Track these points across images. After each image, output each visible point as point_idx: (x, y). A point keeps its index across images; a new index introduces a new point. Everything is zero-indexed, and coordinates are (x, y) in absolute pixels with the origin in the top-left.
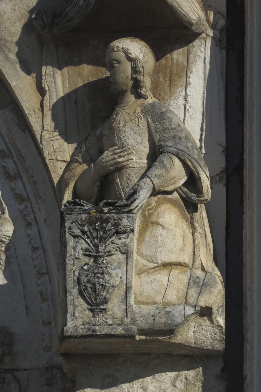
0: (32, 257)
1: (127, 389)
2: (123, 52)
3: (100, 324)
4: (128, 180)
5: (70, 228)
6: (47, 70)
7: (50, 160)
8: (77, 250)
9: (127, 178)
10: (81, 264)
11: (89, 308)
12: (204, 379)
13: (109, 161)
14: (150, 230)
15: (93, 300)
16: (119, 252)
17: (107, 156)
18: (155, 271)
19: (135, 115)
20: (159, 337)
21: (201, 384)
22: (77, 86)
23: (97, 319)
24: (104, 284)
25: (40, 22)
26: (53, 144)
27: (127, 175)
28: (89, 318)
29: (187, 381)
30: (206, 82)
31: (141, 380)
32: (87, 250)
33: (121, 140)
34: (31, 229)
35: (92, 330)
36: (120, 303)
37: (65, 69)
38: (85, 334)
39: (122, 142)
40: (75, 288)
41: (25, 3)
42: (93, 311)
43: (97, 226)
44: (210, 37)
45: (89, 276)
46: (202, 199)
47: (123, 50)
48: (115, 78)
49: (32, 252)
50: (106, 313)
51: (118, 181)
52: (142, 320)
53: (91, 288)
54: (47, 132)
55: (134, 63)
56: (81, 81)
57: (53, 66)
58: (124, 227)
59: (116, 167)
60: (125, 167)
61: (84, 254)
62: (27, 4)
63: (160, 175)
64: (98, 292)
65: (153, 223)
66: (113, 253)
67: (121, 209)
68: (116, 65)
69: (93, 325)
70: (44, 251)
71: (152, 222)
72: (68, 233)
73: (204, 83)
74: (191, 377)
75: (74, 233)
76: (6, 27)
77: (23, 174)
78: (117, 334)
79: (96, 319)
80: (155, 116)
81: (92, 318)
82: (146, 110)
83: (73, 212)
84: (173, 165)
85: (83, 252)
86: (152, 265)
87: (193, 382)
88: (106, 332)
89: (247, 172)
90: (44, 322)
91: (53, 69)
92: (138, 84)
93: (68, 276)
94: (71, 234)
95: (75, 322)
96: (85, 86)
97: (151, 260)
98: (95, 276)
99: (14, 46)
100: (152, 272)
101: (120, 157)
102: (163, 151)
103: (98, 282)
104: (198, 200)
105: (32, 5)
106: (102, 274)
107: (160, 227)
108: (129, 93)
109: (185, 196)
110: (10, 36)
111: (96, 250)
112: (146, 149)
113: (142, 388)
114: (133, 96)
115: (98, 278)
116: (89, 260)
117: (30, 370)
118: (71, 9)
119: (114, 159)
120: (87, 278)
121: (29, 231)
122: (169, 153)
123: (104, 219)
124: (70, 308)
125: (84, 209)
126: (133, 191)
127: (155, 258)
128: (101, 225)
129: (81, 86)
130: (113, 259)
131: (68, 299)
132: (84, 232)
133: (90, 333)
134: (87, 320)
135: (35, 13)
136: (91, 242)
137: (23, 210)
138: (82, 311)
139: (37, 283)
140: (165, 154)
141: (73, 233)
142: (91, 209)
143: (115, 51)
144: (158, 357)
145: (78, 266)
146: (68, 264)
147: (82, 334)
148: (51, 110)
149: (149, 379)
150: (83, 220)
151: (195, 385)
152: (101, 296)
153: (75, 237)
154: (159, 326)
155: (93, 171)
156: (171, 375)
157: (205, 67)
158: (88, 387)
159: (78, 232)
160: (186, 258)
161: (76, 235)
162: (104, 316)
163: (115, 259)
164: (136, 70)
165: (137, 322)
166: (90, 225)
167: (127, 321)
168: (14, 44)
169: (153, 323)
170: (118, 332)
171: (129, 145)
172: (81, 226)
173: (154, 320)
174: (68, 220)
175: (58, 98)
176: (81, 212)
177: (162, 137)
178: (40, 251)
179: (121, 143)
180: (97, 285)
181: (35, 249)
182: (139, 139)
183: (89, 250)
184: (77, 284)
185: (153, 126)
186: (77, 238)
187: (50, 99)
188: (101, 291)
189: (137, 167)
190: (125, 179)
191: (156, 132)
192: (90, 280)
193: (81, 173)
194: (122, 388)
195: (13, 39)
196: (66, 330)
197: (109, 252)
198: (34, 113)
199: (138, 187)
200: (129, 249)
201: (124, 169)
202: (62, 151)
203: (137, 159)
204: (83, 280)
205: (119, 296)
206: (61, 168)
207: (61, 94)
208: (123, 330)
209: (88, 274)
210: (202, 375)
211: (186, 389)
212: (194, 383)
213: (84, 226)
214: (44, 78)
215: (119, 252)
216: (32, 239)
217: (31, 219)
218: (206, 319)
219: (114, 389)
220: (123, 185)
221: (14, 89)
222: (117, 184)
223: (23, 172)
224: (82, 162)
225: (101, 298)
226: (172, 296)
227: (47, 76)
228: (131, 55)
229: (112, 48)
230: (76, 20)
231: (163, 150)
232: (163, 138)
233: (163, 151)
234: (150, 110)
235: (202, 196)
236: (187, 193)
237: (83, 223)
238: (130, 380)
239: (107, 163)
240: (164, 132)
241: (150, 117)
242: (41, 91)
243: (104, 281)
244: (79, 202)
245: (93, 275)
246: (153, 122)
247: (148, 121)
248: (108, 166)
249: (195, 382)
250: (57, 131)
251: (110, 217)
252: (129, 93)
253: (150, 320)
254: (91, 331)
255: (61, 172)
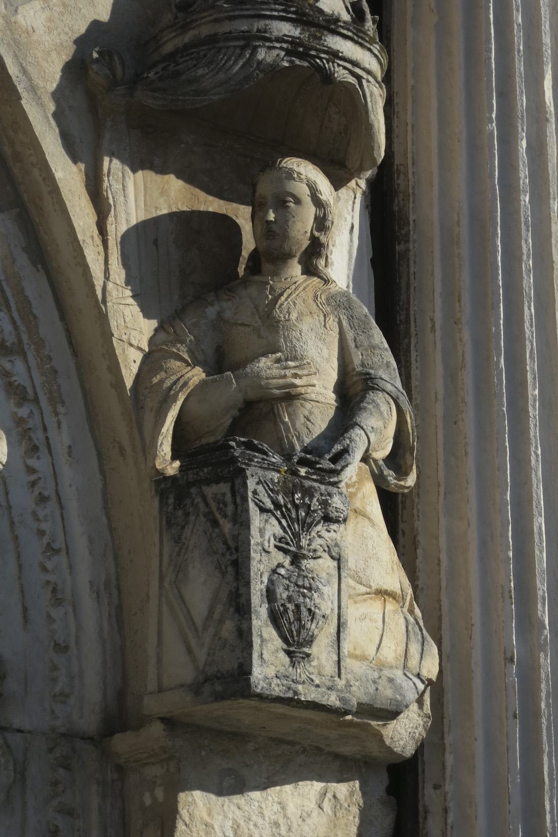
0: (34, 514)
1: (258, 802)
2: (308, 185)
3: (304, 681)
4: (308, 423)
5: (255, 492)
6: (112, 167)
7: (119, 342)
8: (266, 535)
9: (305, 417)
10: (272, 563)
11: (284, 648)
12: (365, 803)
13: (275, 378)
14: (353, 523)
15: (295, 635)
16: (326, 555)
18: (365, 600)
19: (318, 306)
20: (372, 721)
21: (358, 811)
22: (160, 213)
23: (298, 670)
24: (313, 609)
25: (108, 72)
26: (124, 312)
27: (306, 413)
28: (284, 666)
29: (336, 802)
30: (352, 268)
31: (278, 788)
32: (283, 540)
33: (292, 344)
34: (38, 458)
35: (293, 690)
36: (330, 649)
37: (140, 174)
38: (282, 695)
39: (294, 349)
40: (263, 605)
41: (68, 22)
42: (292, 655)
43: (297, 499)
44: (361, 190)
45: (291, 589)
46: (402, 483)
47: (307, 181)
48: (287, 227)
49: (37, 504)
50: (309, 662)
51: (287, 420)
52: (358, 687)
53: (293, 611)
54: (113, 286)
55: (322, 211)
56: (166, 206)
57: (123, 161)
58: (337, 512)
59: (286, 392)
60: (302, 396)
61: (276, 546)
62: (70, 24)
63: (377, 428)
64: (303, 622)
65: (356, 512)
66: (319, 554)
67: (324, 476)
68: (292, 205)
69: (293, 681)
70: (62, 507)
71: (355, 510)
72: (252, 500)
73: (349, 269)
74: (342, 796)
75: (263, 503)
76: (35, 58)
77: (28, 349)
78: (329, 705)
79: (297, 672)
80: (355, 317)
81: (289, 667)
82: (336, 302)
83: (253, 463)
84: (390, 416)
85: (275, 542)
86: (363, 589)
87: (346, 805)
88: (314, 698)
90: (56, 645)
91: (123, 167)
92: (318, 249)
93: (253, 581)
94: (256, 504)
95: (264, 671)
96: (172, 215)
97: (357, 579)
98: (299, 591)
99: (48, 100)
100: (360, 601)
101: (295, 376)
102: (376, 386)
103: (303, 603)
104: (396, 483)
105: (79, 30)
106: (310, 589)
107: (367, 522)
108: (296, 260)
109: (377, 472)
110: (42, 77)
111: (296, 543)
113: (280, 803)
114: (299, 267)
115: (304, 596)
116: (283, 558)
117: (30, 732)
118: (207, 74)
119: (285, 376)
120: (287, 593)
121: (32, 462)
122: (384, 393)
123: (306, 488)
124: (256, 641)
125: (270, 461)
126: (342, 448)
127: (365, 576)
128: (303, 498)
129: (164, 215)
130: (319, 565)
131: (253, 625)
132: (277, 505)
133: (290, 695)
134: (282, 670)
135: (97, 49)
136: (289, 526)
137: (27, 418)
138: (274, 651)
139: (44, 566)
140: (378, 392)
141: (261, 503)
142: (281, 465)
143: (294, 179)
144: (304, 751)
145: (267, 566)
146: (254, 559)
147: (277, 694)
148: (119, 245)
149: (288, 788)
150: (275, 483)
151: (349, 811)
152: (307, 629)
153: (263, 510)
154: (383, 701)
155: (235, 388)
156: (318, 786)
157: (351, 240)
158: (198, 789)
159: (269, 505)
161: (268, 508)
162: (307, 667)
163: (322, 566)
164: (324, 225)
165: (351, 689)
166: (286, 494)
167: (341, 683)
168: (49, 95)
169: (376, 695)
170: (331, 701)
171: (308, 358)
172: (272, 493)
173: (377, 689)
174: (252, 476)
175: (129, 227)
176: (266, 466)
177: (367, 360)
178: (52, 506)
179: (291, 351)
180: (303, 609)
181: (42, 499)
182: (325, 352)
183: (287, 540)
184: (266, 600)
185: (350, 335)
186: (266, 514)
187: (116, 223)
188: (308, 621)
189: (322, 403)
190: (302, 420)
191: (356, 347)
192: (291, 596)
193: (197, 383)
194: (251, 799)
195: (46, 84)
196: (255, 682)
197: (315, 551)
198: (91, 242)
199: (351, 442)
200: (343, 554)
201: (299, 399)
202: (137, 329)
203: (321, 386)
204: (281, 595)
205: (328, 636)
206: (135, 362)
207: (134, 222)
208: (338, 699)
209: (288, 586)
210: (361, 795)
211: (335, 817)
212: (347, 807)
213: (277, 493)
214: (106, 179)
215: (327, 554)
216: (40, 478)
217: (38, 439)
219: (238, 799)
220: (298, 430)
221: (60, 185)
222: (285, 424)
223: (28, 344)
224: (190, 362)
225: (307, 635)
227: (111, 178)
228: (322, 195)
229: (288, 172)
230: (213, 97)
231: (375, 384)
232: (370, 363)
233: (376, 386)
234: (345, 304)
235: (404, 479)
236: (382, 467)
237: (275, 487)
238: (264, 787)
239: (269, 381)
240: (371, 351)
241: (345, 317)
243: (312, 604)
244: (260, 446)
245: (297, 589)
246: (351, 328)
247: (342, 325)
248: (271, 387)
249: (349, 806)
250: (129, 288)
251: (315, 487)
252: (296, 260)
253: (372, 690)
254: (292, 691)
255: (135, 369)
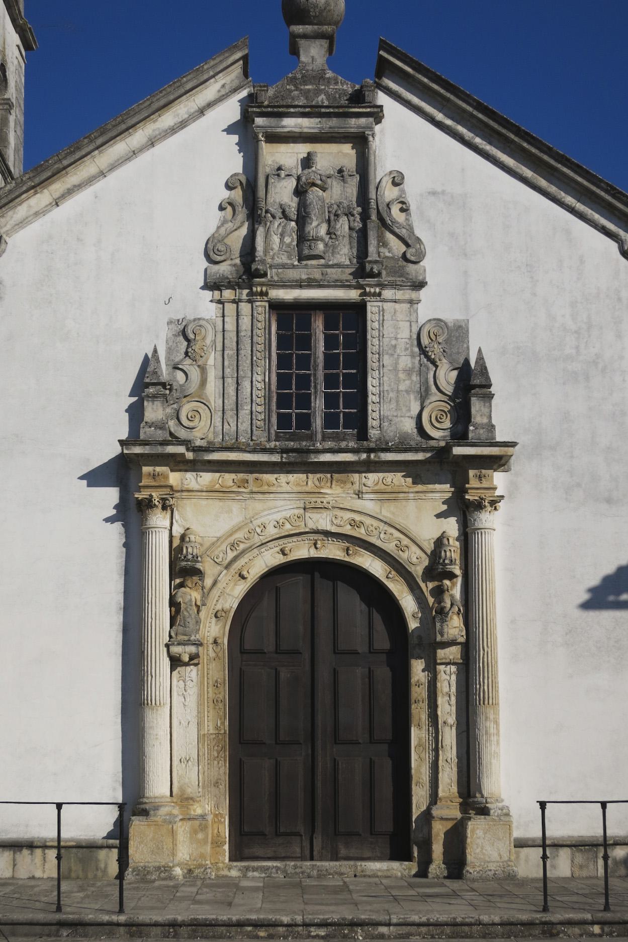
6: (428, 583)
17: (442, 604)
89: (329, 765)
112: (450, 603)
160: (458, 626)
218: (30, 207)
226: (456, 633)
242: (427, 587)
